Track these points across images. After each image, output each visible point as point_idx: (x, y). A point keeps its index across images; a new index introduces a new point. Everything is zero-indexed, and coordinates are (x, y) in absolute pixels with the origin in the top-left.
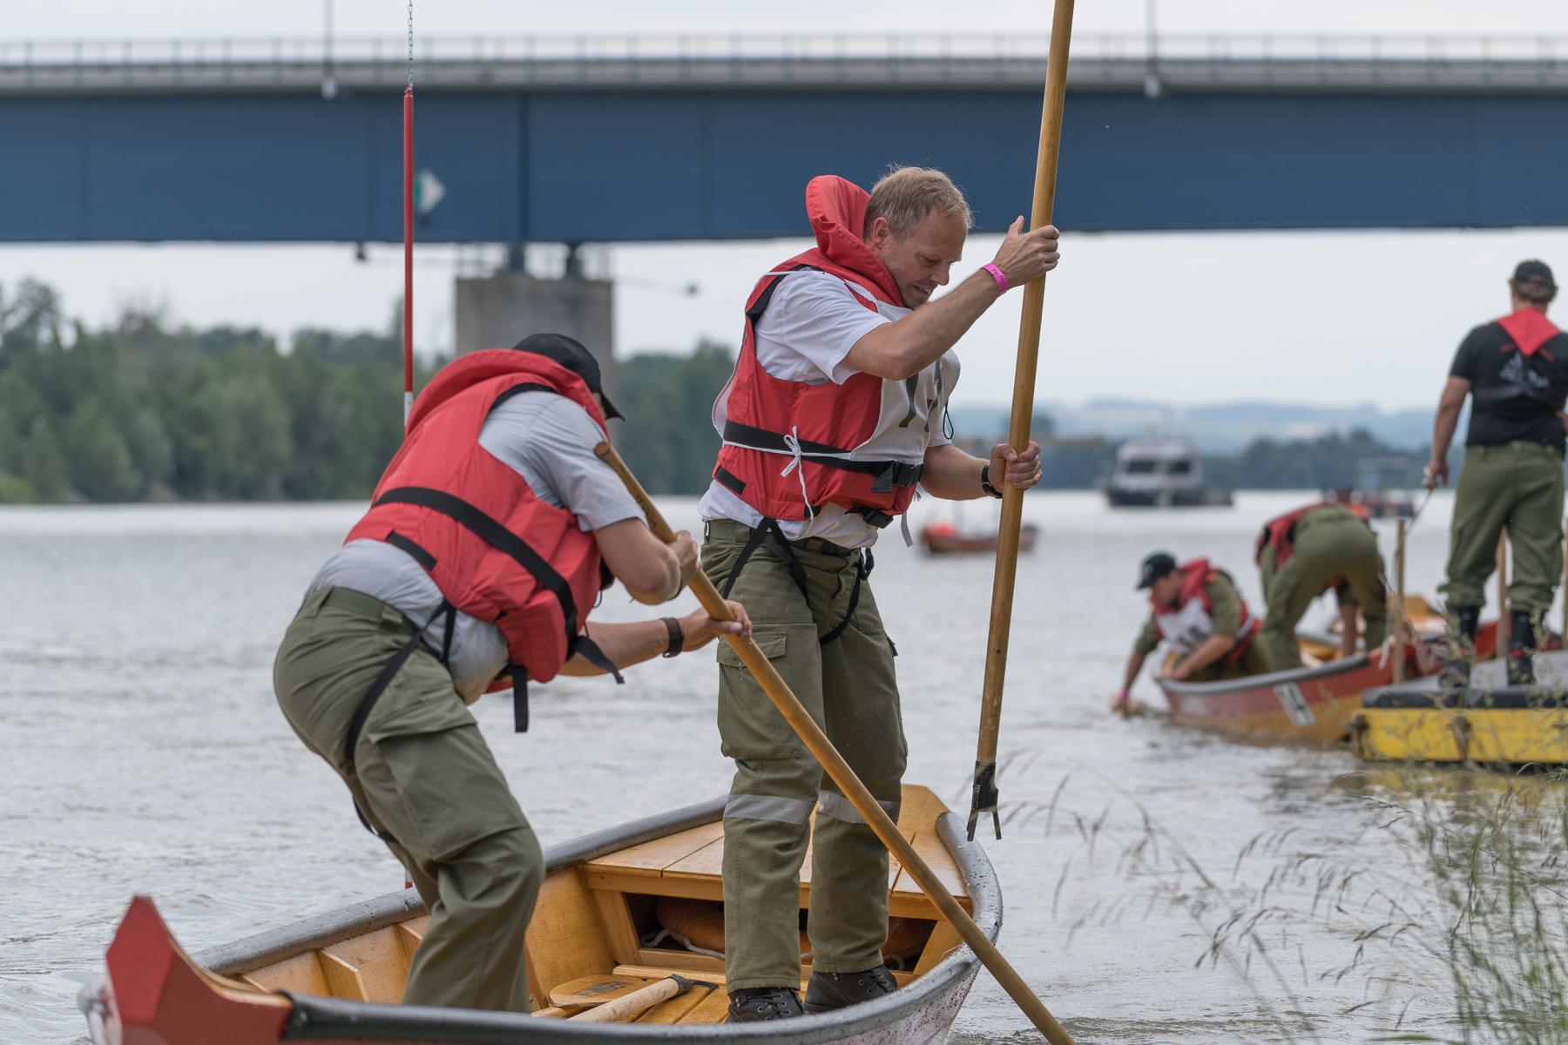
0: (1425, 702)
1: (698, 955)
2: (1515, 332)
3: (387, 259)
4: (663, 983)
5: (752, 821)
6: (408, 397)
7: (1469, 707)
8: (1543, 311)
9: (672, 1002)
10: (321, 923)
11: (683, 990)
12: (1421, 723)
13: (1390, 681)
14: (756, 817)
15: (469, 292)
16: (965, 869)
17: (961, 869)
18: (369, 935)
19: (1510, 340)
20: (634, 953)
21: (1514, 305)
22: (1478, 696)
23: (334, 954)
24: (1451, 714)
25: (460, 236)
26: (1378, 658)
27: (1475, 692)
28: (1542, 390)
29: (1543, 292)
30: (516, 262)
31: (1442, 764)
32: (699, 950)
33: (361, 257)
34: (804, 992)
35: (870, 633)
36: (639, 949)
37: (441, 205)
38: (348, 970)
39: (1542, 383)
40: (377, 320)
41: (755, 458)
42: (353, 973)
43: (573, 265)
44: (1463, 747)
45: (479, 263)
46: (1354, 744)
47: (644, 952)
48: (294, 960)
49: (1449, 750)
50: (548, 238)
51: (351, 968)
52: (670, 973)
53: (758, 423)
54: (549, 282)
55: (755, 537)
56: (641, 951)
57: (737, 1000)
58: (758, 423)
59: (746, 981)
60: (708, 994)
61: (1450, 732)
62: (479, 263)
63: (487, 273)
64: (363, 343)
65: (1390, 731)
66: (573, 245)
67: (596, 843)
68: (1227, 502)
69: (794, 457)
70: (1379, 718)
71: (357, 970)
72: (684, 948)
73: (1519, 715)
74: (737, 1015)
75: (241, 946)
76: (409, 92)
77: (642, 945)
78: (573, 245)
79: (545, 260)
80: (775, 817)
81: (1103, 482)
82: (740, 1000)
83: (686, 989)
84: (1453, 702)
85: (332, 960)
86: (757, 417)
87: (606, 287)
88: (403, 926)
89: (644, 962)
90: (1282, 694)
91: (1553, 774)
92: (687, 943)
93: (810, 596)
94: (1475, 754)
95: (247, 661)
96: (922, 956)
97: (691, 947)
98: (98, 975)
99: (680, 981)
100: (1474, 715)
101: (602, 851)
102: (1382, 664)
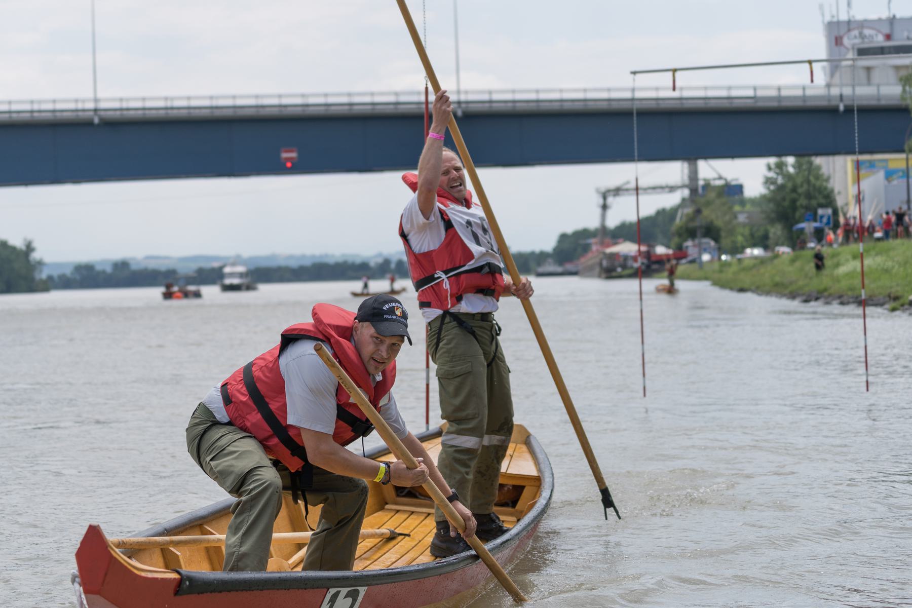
5: (457, 447)
35: (501, 362)
41: (427, 291)
53: (425, 275)
55: (443, 317)
57: (442, 531)
58: (425, 275)
67: (376, 451)
68: (827, 303)
69: (443, 280)
77: (398, 496)
82: (443, 531)
86: (424, 274)
92: (417, 494)
93: (477, 337)
95: (86, 526)
97: (420, 497)
98: (73, 567)
101: (380, 454)
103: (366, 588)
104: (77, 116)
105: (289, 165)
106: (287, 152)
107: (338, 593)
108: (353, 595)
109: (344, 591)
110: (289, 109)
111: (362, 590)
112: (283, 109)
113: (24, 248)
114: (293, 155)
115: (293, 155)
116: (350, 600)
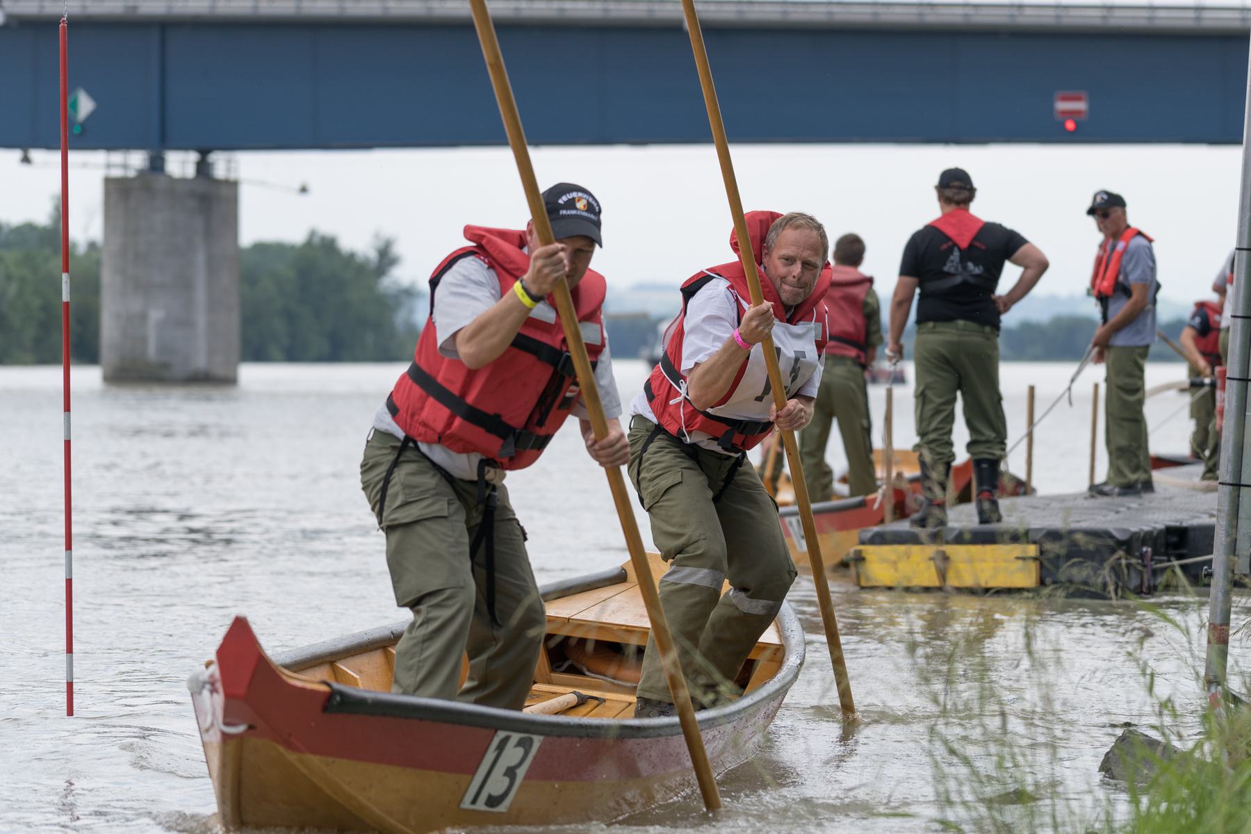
0: (913, 539)
1: (591, 678)
2: (950, 231)
3: (46, 160)
4: (568, 696)
5: (676, 584)
6: (65, 277)
7: (948, 543)
8: (967, 209)
9: (572, 710)
10: (335, 644)
11: (581, 702)
12: (908, 555)
13: (882, 521)
14: (678, 582)
15: (116, 190)
16: (781, 625)
17: (779, 626)
18: (367, 654)
19: (948, 239)
20: (547, 675)
21: (942, 208)
22: (955, 533)
23: (342, 666)
24: (931, 550)
25: (110, 145)
26: (874, 500)
27: (953, 529)
28: (977, 276)
29: (964, 194)
30: (157, 165)
31: (927, 590)
32: (593, 675)
33: (26, 160)
34: (580, 720)
36: (551, 672)
37: (92, 116)
38: (353, 677)
39: (978, 270)
40: (42, 215)
42: (356, 679)
43: (203, 168)
44: (943, 575)
45: (125, 166)
46: (853, 571)
47: (554, 675)
48: (317, 669)
49: (931, 579)
50: (182, 146)
51: (355, 675)
52: (572, 690)
54: (183, 181)
56: (552, 674)
59: (646, 693)
60: (598, 706)
61: (932, 563)
62: (125, 166)
63: (131, 174)
64: (27, 231)
65: (884, 560)
66: (204, 152)
70: (871, 551)
71: (358, 677)
72: (583, 674)
73: (989, 548)
74: (639, 714)
75: (283, 656)
76: (64, 21)
77: (553, 670)
78: (204, 152)
79: (180, 164)
80: (691, 581)
81: (645, 352)
83: (582, 701)
84: (935, 538)
85: (341, 669)
87: (232, 186)
88: (389, 649)
89: (554, 682)
90: (791, 523)
91: (1017, 596)
92: (585, 669)
94: (952, 581)
96: (749, 685)
97: (587, 673)
99: (579, 695)
100: (950, 550)
102: (876, 506)
103: (541, 738)
104: (562, 10)
105: (1070, 125)
106: (1065, 99)
107: (506, 739)
108: (525, 744)
109: (515, 737)
110: (985, 11)
111: (537, 740)
112: (927, 10)
113: (373, 255)
114: (1081, 106)
115: (1081, 106)
116: (520, 751)
